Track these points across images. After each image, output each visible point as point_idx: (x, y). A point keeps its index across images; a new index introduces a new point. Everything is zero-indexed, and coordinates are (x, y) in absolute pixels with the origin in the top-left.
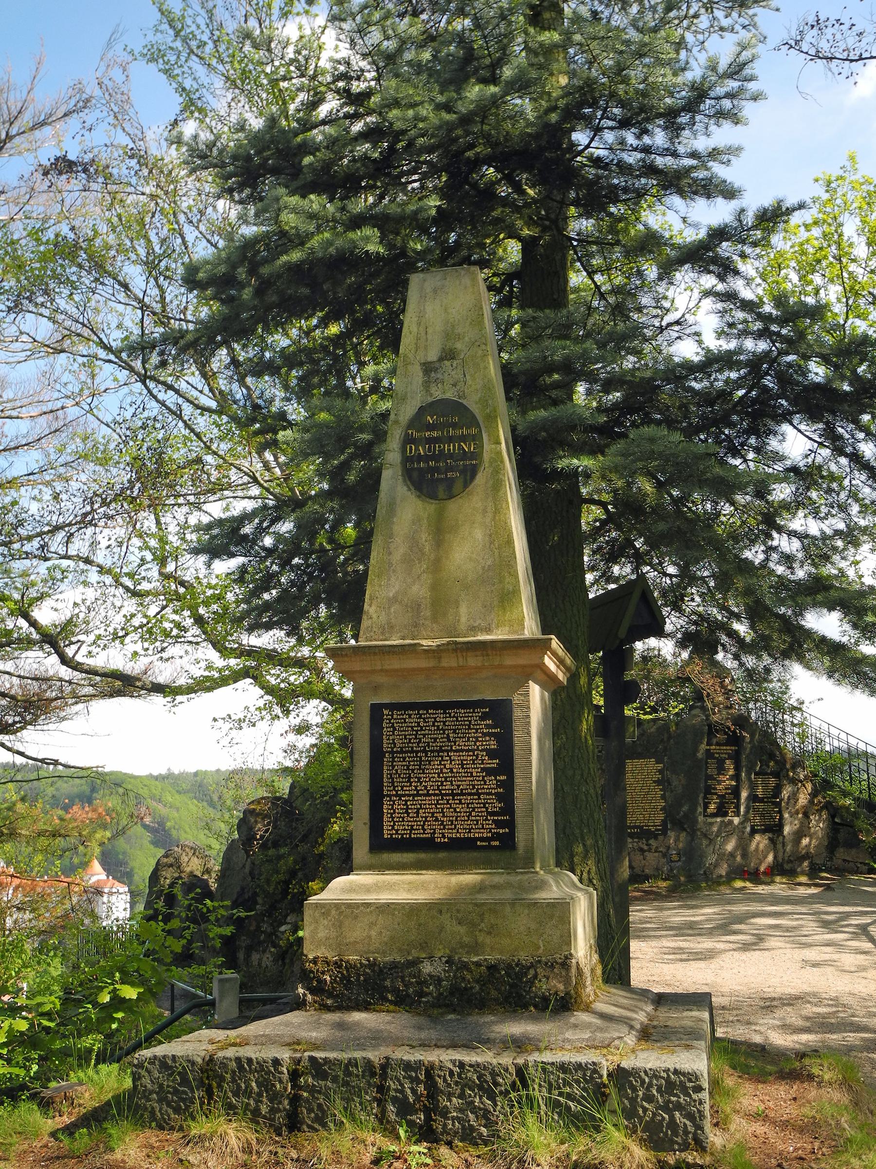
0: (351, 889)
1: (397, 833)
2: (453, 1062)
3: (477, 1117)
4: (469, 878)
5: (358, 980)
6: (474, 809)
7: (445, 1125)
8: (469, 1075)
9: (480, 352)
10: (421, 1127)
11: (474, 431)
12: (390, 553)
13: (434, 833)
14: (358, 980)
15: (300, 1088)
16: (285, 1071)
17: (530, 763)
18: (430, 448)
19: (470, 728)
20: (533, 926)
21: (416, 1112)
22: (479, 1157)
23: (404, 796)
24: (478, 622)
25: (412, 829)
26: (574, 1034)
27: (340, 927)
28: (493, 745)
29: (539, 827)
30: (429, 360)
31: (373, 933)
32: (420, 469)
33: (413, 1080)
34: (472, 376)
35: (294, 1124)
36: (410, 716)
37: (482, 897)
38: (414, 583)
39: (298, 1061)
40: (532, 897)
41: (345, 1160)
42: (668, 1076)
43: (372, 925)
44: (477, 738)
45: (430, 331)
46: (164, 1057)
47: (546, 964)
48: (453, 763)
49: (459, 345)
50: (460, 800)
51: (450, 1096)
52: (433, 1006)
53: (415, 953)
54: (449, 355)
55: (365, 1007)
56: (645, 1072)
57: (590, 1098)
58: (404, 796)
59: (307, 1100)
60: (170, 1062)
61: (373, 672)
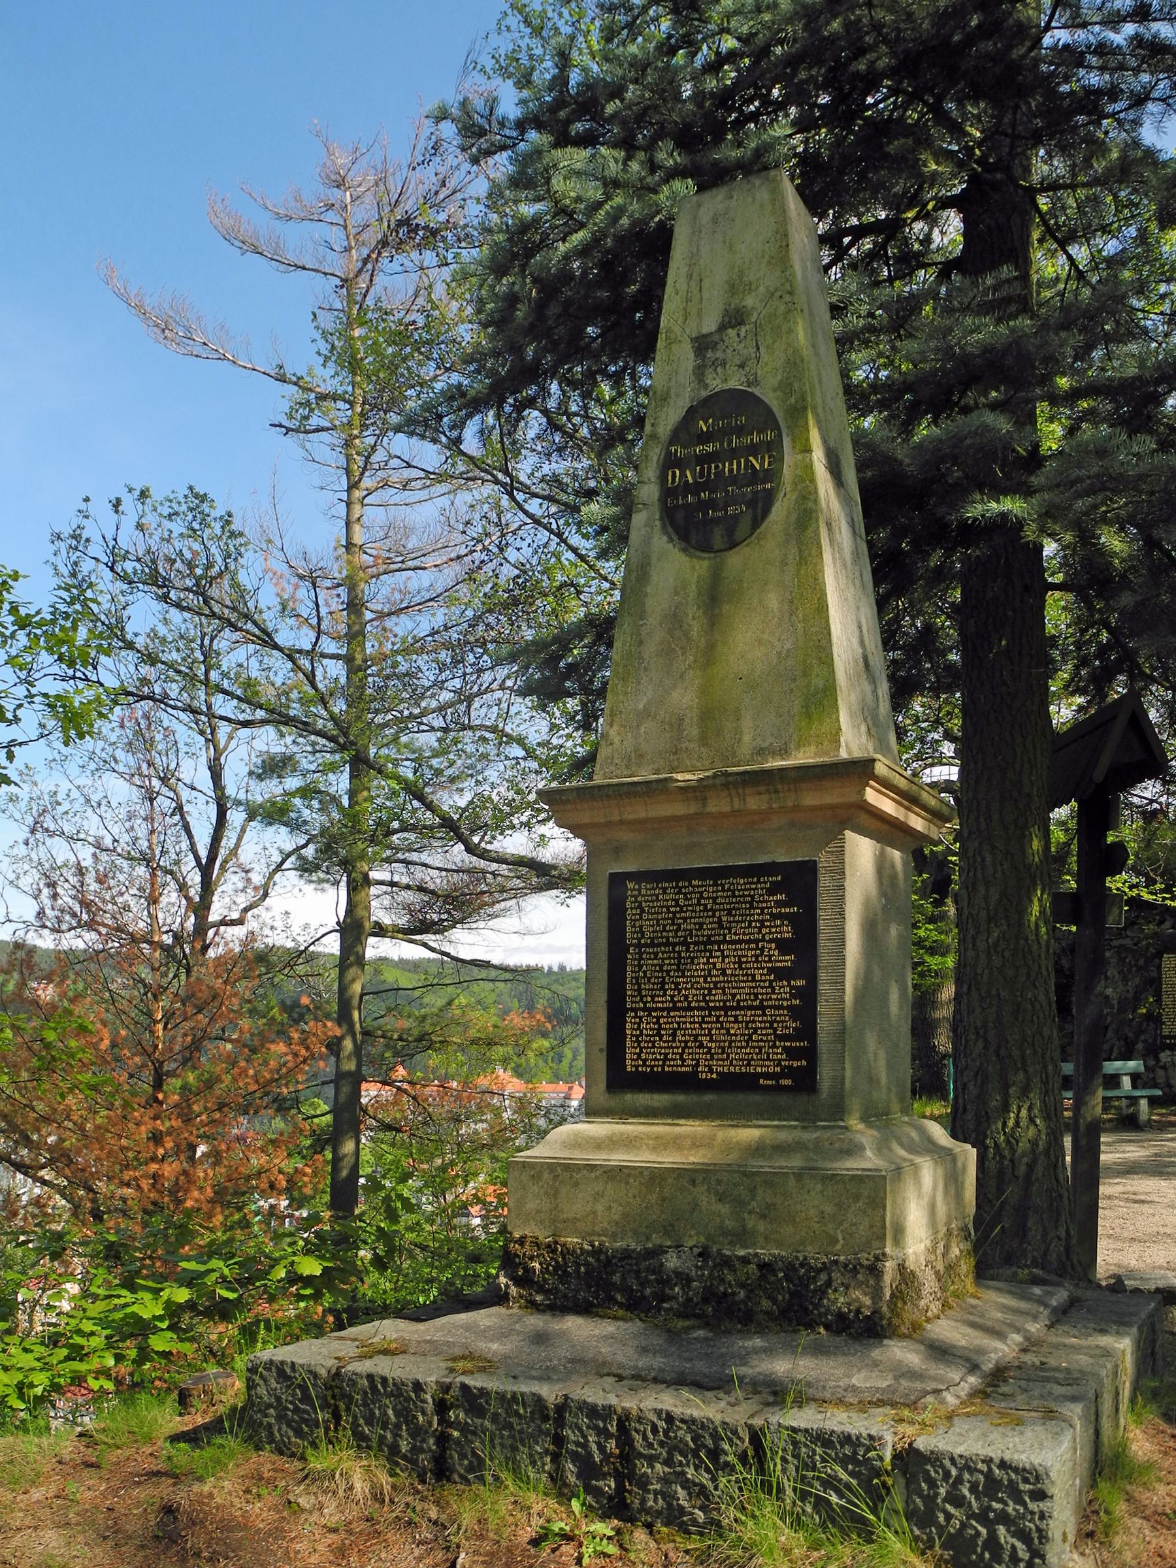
0: (576, 1143)
1: (644, 1065)
2: (658, 1412)
3: (690, 1494)
4: (748, 1134)
5: (577, 1271)
6: (755, 1032)
7: (643, 1501)
8: (680, 1433)
9: (782, 308)
10: (610, 1498)
11: (770, 435)
12: (641, 643)
13: (697, 1065)
14: (577, 1271)
15: (450, 1425)
16: (430, 1400)
17: (843, 959)
18: (702, 470)
19: (752, 907)
20: (829, 1209)
21: (604, 1476)
22: (687, 1552)
23: (655, 1010)
24: (770, 740)
25: (666, 1059)
26: (866, 1379)
27: (555, 1196)
28: (787, 932)
29: (875, 1057)
30: (705, 331)
31: (599, 1208)
32: (687, 506)
33: (603, 1433)
34: (768, 347)
35: (442, 1471)
36: (664, 890)
37: (763, 1165)
38: (675, 687)
39: (446, 1388)
40: (829, 1165)
41: (491, 1535)
42: (990, 1469)
43: (598, 1196)
44: (762, 922)
45: (706, 284)
46: (282, 1363)
47: (846, 1266)
48: (726, 960)
49: (749, 301)
50: (736, 1017)
51: (651, 1460)
52: (680, 1315)
53: (656, 1240)
54: (734, 319)
55: (584, 1309)
56: (952, 1459)
57: (863, 1487)
58: (655, 1010)
59: (458, 1442)
60: (288, 1370)
61: (609, 824)
